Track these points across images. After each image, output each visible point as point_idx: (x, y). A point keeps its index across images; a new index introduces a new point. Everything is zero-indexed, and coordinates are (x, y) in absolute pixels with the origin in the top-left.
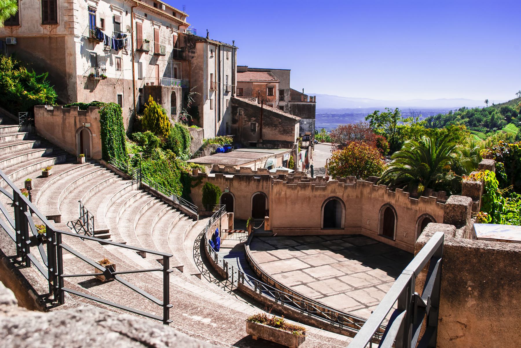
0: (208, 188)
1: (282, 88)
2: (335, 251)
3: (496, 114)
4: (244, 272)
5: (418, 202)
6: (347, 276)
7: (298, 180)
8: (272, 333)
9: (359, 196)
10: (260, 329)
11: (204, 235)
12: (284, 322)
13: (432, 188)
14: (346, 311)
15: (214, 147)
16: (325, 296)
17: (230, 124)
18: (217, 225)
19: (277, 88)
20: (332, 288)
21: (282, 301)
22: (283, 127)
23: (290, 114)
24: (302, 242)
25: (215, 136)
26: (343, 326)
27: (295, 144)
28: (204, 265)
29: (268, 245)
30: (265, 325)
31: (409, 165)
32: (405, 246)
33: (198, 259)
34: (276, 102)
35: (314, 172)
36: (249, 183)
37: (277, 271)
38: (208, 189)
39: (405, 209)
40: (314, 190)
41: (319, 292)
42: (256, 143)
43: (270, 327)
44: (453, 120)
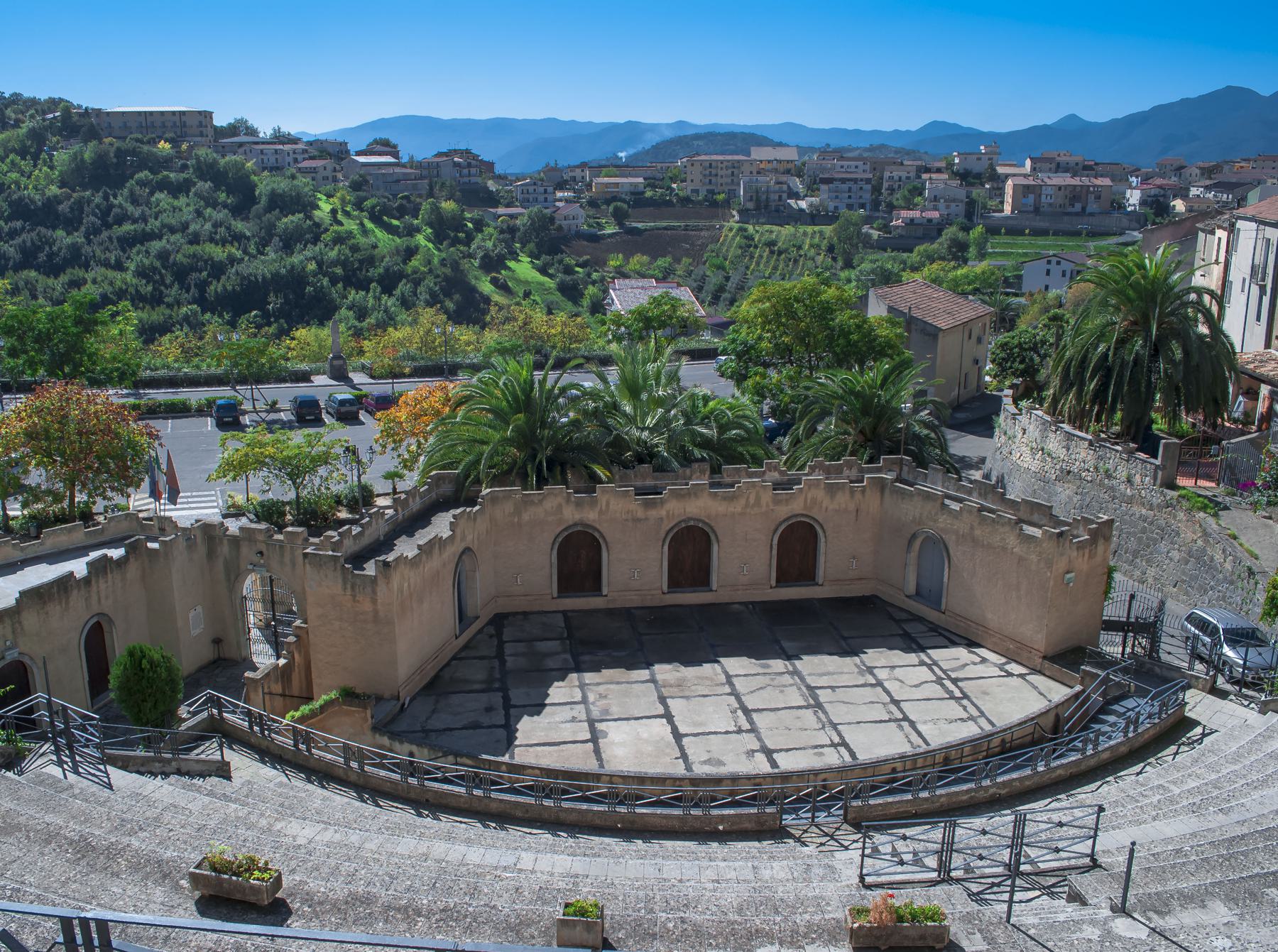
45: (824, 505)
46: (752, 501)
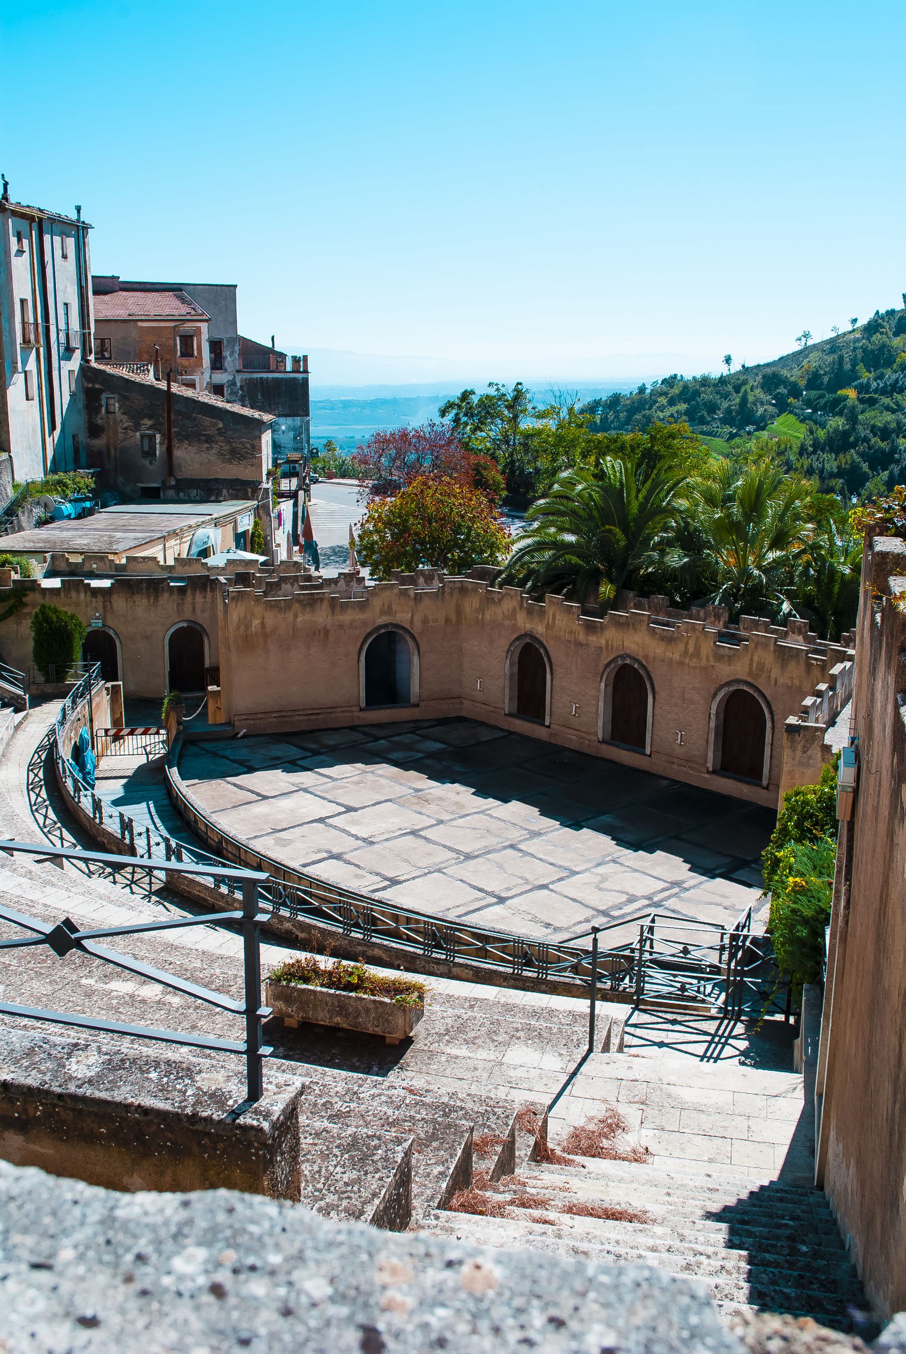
0: (47, 619)
1: (217, 336)
2: (404, 765)
3: (752, 390)
4: (168, 836)
5: (602, 627)
6: (441, 826)
7: (292, 585)
8: (339, 1006)
9: (453, 618)
10: (304, 999)
11: (52, 748)
12: (367, 975)
13: (633, 590)
14: (451, 916)
15: (46, 506)
16: (394, 882)
17: (82, 438)
18: (82, 720)
19: (205, 336)
20: (407, 861)
21: (292, 908)
22: (230, 443)
23: (243, 406)
24: (314, 746)
25: (46, 474)
26: (454, 957)
27: (265, 485)
28: (63, 829)
29: (227, 762)
30: (319, 989)
31: (573, 533)
32: (574, 738)
33: (46, 817)
34: (204, 375)
35: (321, 558)
36: (156, 598)
37: (261, 830)
38: (47, 622)
39: (572, 647)
40: (338, 609)
41: (377, 874)
42: (158, 488)
43: (332, 991)
44: (650, 409)
45: (773, 676)
46: (691, 649)
